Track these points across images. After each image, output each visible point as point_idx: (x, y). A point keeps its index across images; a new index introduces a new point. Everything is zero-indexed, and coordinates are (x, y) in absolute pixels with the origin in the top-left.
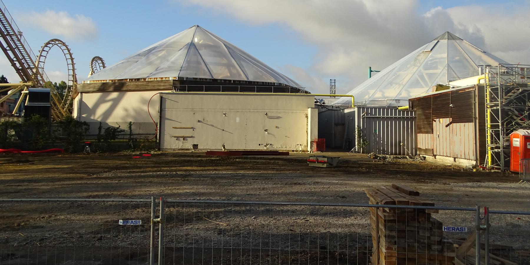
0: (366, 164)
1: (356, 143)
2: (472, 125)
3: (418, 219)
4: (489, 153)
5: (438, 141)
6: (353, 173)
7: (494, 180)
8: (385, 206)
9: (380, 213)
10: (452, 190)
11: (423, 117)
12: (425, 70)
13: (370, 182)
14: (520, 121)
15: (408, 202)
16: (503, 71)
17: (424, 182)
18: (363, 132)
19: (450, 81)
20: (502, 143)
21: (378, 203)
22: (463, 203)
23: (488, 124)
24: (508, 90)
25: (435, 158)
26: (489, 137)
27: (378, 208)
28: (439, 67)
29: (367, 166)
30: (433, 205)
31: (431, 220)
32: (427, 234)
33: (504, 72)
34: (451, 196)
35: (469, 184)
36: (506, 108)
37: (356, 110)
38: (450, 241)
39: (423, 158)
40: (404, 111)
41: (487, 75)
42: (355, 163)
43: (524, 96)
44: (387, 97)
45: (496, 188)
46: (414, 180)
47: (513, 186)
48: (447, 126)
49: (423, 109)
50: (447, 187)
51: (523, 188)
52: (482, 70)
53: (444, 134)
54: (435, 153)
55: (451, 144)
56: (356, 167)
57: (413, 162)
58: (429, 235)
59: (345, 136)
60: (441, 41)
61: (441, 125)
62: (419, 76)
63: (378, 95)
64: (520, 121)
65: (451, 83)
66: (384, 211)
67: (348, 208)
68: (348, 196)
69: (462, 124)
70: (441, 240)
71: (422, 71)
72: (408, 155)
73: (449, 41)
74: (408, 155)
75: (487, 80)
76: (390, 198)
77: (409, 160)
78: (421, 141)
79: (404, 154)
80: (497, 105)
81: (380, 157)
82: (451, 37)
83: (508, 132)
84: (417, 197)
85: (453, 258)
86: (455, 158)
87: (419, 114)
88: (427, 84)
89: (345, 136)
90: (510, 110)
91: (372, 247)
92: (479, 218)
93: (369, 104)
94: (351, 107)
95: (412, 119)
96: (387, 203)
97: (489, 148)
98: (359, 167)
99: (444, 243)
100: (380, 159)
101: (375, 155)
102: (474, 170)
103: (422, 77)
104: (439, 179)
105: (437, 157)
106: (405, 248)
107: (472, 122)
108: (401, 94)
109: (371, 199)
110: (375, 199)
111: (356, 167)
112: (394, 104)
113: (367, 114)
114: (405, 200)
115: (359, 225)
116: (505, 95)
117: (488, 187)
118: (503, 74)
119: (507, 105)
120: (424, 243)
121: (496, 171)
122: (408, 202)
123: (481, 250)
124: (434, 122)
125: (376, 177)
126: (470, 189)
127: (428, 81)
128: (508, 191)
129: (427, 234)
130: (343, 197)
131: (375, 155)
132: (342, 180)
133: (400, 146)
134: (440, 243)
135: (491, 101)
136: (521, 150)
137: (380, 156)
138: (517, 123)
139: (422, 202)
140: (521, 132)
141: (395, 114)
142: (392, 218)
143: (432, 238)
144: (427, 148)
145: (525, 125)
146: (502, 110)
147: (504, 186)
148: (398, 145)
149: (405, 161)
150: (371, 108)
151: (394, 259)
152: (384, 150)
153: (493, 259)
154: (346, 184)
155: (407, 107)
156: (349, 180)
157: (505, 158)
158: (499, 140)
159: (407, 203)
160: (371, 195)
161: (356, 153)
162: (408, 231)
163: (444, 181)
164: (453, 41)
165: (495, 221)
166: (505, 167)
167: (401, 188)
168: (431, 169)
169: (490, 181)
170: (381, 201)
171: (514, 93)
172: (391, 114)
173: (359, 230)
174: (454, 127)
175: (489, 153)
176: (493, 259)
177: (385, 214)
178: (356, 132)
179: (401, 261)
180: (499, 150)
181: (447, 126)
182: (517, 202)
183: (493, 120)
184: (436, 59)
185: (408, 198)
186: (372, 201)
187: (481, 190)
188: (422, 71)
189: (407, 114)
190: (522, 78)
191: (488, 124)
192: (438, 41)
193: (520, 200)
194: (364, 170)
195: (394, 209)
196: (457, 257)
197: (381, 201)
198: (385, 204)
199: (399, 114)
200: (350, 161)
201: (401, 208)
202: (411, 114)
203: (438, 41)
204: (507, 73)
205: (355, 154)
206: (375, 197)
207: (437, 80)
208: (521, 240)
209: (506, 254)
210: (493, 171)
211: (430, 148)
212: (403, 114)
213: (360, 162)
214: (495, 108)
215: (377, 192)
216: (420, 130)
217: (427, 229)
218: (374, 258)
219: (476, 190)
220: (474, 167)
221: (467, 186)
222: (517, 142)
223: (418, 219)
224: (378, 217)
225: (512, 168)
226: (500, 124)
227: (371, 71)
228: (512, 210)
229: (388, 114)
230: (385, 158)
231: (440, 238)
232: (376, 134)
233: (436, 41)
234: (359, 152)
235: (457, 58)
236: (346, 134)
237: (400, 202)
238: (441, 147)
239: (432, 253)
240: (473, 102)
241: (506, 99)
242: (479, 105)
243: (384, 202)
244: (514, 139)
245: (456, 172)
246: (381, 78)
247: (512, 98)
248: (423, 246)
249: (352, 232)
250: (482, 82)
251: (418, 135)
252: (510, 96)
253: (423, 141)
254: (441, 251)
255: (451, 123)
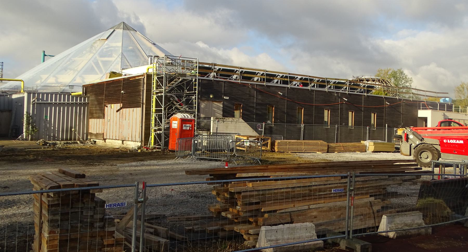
0: (34, 151)
1: (24, 130)
2: (139, 110)
3: (82, 200)
4: (153, 134)
5: (109, 126)
6: (19, 161)
7: (155, 159)
8: (50, 191)
9: (44, 199)
10: (118, 170)
11: (96, 103)
12: (101, 57)
13: (37, 169)
14: (178, 106)
15: (74, 184)
16: (168, 62)
17: (92, 165)
18: (32, 118)
19: (123, 69)
20: (163, 125)
21: (42, 189)
22: (126, 181)
23: (153, 109)
24: (171, 79)
25: (105, 142)
26: (153, 121)
27: (42, 194)
28: (114, 55)
29: (35, 153)
30: (98, 185)
31: (95, 199)
32: (90, 213)
33: (169, 63)
34: (118, 176)
35: (134, 164)
36: (169, 94)
37: (26, 95)
38: (112, 216)
39: (93, 143)
40: (77, 97)
41: (155, 65)
42: (21, 150)
43: (183, 84)
44: (61, 83)
45: (156, 165)
46: (83, 164)
47: (169, 163)
48: (117, 111)
49: (95, 94)
50: (114, 168)
51: (177, 164)
52: (151, 60)
53: (115, 118)
54: (105, 137)
55: (120, 128)
56: (22, 155)
57: (84, 147)
58: (92, 214)
59: (12, 124)
60: (117, 30)
61: (112, 110)
62: (94, 63)
63: (51, 81)
64: (178, 106)
65: (123, 71)
66: (48, 196)
67: (10, 198)
68: (12, 185)
69: (131, 109)
70: (104, 217)
71: (98, 58)
72: (79, 140)
73: (125, 31)
74: (79, 140)
75: (155, 69)
76: (56, 182)
77: (79, 145)
78: (93, 126)
79: (75, 139)
80: (161, 92)
81: (50, 144)
82: (126, 27)
83: (169, 116)
84: (83, 179)
85: (113, 232)
86: (123, 141)
87: (92, 100)
88: (101, 71)
89: (12, 124)
90: (172, 96)
91: (34, 234)
92: (138, 192)
93: (40, 89)
94: (20, 92)
95: (85, 105)
96: (51, 188)
97: (153, 130)
98: (26, 155)
99: (106, 219)
100: (50, 146)
101: (45, 142)
102: (139, 151)
103: (97, 64)
104: (107, 161)
105: (107, 141)
106: (67, 230)
107: (140, 107)
108: (75, 80)
109: (36, 185)
110: (39, 185)
111: (22, 155)
112: (68, 89)
113: (38, 99)
114: (70, 183)
115: (22, 214)
116: (169, 83)
117: (150, 165)
118: (168, 64)
119: (170, 92)
120: (87, 222)
121: (158, 150)
122: (74, 184)
123: (138, 220)
124: (106, 107)
125: (44, 164)
126: (134, 168)
127: (103, 68)
128: (165, 167)
129: (90, 213)
130: (5, 187)
131: (45, 142)
132: (5, 170)
133: (71, 131)
134: (102, 220)
135: (157, 89)
136: (178, 131)
137: (50, 142)
138: (177, 108)
139: (87, 183)
140: (179, 116)
141: (68, 100)
142: (56, 203)
143: (95, 216)
144: (98, 132)
145: (182, 109)
146: (165, 96)
147: (162, 163)
148: (70, 130)
149: (76, 146)
150: (43, 94)
151: (57, 242)
152: (54, 136)
153: (148, 227)
154: (10, 173)
155: (81, 93)
156: (13, 169)
157: (165, 138)
158: (161, 123)
159: (73, 186)
160: (35, 182)
161: (25, 140)
162: (72, 213)
163: (111, 163)
164: (128, 31)
165: (152, 195)
166: (164, 146)
167: (68, 172)
168: (101, 152)
169: (151, 160)
170: (46, 187)
171: (176, 81)
172: (64, 100)
173: (22, 219)
174: (124, 112)
175: (153, 134)
176: (148, 227)
177: (50, 199)
178: (25, 119)
179: (63, 243)
180: (161, 132)
181: (117, 111)
182: (171, 176)
183: (158, 105)
184: (112, 47)
185: (74, 181)
186: (37, 187)
187: (144, 168)
188: (98, 58)
189: (81, 100)
190: (182, 69)
191: (153, 109)
192: (114, 30)
193: (174, 174)
194: (31, 157)
195: (58, 193)
196: (118, 230)
197: (46, 187)
198: (49, 189)
199: (72, 100)
200: (16, 149)
201: (66, 191)
202: (84, 100)
203: (114, 30)
204: (172, 64)
205: (22, 142)
206: (40, 183)
207: (111, 67)
208: (172, 207)
209: (159, 222)
210: (154, 150)
211: (100, 132)
212: (76, 100)
213: (27, 150)
214: (160, 94)
215: (43, 177)
216: (92, 115)
217: (91, 208)
218: (35, 245)
219: (139, 168)
220: (139, 148)
221: (132, 166)
222: (175, 125)
223: (82, 200)
224: (41, 203)
225: (170, 148)
226: (163, 109)
227: (45, 55)
228: (167, 183)
229: (62, 100)
230: (55, 144)
231: (103, 215)
232: (47, 120)
233: (113, 30)
234: (26, 140)
235: (131, 48)
236: (13, 121)
237: (65, 186)
238: (111, 129)
239: (94, 230)
240: (142, 89)
241: (169, 87)
242: (146, 92)
243: (48, 187)
244: (174, 122)
245: (122, 154)
246: (55, 63)
247: (174, 86)
248: (86, 226)
249: (14, 222)
250: (151, 71)
251: (90, 120)
252: (173, 84)
253: (95, 125)
254: (104, 227)
255: (121, 108)
